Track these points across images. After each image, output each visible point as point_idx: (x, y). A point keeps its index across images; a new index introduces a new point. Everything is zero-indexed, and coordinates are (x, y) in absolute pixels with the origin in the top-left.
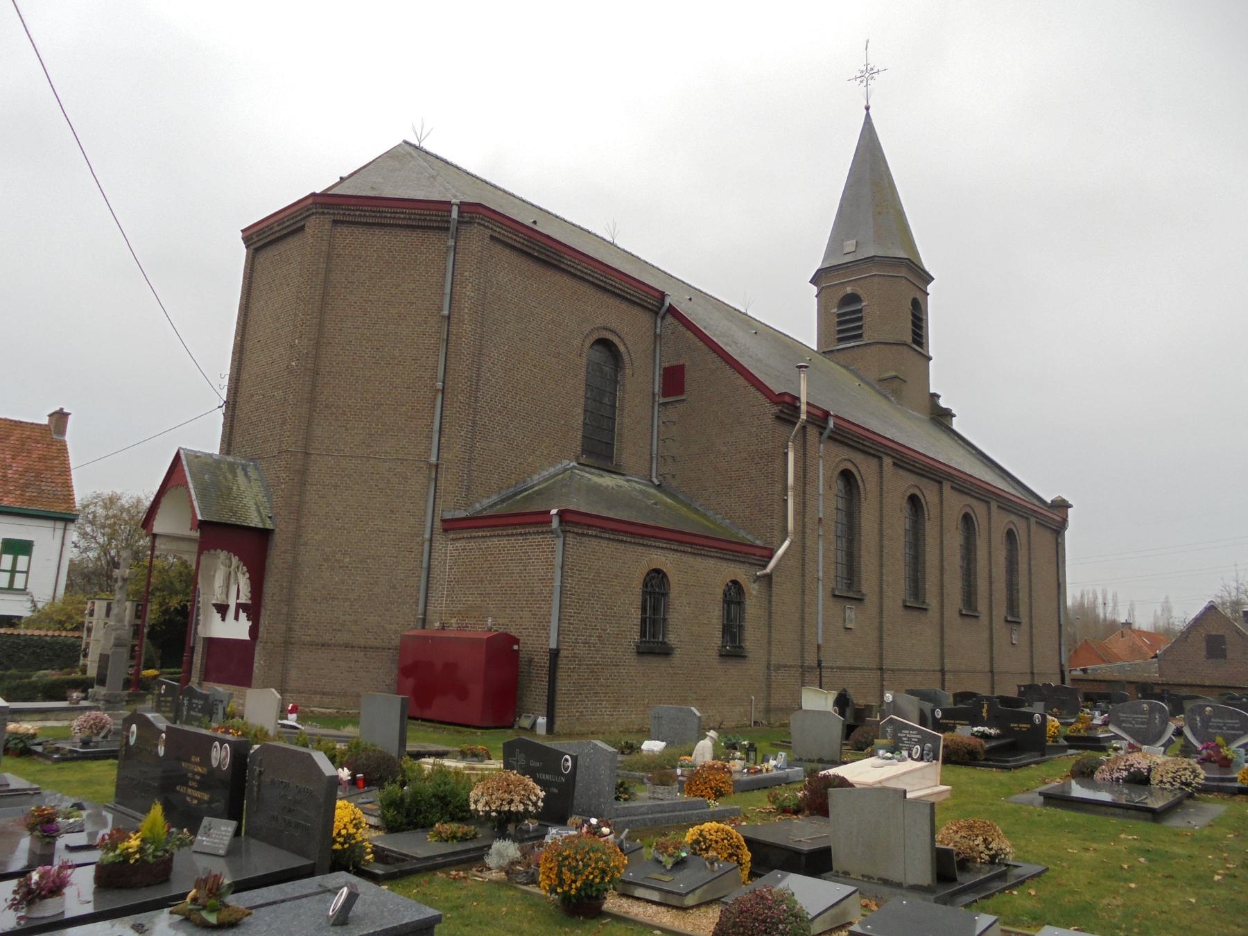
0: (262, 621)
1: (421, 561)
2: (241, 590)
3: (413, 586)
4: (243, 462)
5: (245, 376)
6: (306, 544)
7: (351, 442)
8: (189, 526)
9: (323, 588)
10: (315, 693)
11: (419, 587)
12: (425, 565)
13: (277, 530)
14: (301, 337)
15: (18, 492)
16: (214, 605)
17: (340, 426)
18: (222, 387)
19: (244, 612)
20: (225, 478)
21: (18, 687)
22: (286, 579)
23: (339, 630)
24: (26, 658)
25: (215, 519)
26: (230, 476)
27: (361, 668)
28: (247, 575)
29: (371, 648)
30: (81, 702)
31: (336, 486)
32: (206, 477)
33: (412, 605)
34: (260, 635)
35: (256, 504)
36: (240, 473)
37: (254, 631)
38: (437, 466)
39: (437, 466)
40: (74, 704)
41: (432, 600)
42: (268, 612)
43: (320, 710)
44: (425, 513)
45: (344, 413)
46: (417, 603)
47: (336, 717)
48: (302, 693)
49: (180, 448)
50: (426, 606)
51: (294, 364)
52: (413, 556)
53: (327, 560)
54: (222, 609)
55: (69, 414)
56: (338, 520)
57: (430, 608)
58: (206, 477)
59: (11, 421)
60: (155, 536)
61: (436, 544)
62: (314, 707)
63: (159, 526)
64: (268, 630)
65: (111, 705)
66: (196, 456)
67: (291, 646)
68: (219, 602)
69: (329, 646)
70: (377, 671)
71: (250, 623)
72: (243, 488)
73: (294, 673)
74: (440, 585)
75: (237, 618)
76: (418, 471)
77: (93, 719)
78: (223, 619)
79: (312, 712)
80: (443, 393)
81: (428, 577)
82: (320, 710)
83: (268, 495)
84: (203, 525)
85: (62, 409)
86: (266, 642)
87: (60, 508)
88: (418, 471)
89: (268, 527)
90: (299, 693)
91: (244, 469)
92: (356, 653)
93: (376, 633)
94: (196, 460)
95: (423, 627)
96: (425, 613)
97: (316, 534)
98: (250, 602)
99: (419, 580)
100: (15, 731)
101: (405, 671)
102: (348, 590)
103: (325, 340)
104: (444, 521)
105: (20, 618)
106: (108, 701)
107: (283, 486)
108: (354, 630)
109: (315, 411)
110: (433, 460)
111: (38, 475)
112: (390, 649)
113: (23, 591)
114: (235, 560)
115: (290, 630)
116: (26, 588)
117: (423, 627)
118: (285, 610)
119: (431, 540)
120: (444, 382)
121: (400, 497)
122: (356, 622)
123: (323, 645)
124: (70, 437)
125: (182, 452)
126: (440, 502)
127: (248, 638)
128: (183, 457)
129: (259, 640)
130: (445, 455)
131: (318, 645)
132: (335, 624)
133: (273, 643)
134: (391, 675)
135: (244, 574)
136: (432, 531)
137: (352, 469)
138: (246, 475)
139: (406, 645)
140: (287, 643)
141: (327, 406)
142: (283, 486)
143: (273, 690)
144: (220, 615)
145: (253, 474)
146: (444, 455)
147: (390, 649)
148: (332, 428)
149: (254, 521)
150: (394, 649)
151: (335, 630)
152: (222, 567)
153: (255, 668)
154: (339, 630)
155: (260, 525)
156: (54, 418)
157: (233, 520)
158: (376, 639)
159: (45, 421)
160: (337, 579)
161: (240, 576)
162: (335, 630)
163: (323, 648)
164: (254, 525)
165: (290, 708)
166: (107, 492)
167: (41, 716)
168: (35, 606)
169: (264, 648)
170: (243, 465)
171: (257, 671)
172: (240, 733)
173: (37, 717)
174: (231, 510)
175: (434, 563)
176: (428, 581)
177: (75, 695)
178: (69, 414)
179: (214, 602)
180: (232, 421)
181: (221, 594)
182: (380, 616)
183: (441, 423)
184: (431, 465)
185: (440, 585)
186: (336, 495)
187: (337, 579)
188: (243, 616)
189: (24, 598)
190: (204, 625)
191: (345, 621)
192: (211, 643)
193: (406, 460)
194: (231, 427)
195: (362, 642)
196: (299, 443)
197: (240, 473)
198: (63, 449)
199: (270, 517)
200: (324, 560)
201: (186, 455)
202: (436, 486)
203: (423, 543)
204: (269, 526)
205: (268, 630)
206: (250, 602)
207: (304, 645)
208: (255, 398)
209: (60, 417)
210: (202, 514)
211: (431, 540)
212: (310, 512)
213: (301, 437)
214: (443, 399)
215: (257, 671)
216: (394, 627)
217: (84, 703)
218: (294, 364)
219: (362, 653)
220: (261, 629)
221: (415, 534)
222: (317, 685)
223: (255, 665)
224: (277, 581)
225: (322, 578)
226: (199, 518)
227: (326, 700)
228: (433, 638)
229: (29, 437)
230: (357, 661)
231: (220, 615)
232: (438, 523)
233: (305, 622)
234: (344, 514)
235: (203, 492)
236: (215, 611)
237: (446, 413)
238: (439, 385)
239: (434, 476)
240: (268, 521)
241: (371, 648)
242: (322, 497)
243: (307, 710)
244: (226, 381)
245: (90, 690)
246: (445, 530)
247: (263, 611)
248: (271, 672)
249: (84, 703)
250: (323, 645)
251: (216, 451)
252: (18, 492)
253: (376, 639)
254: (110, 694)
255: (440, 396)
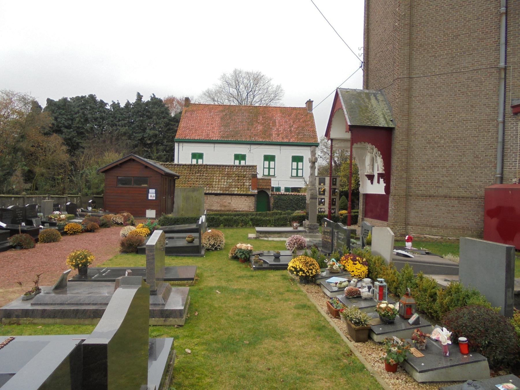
0: (392, 183)
1: (497, 138)
2: (379, 167)
3: (491, 156)
4: (374, 92)
5: (371, 45)
6: (415, 134)
7: (439, 65)
8: (345, 130)
9: (428, 160)
10: (427, 226)
11: (496, 155)
12: (500, 139)
13: (396, 127)
14: (399, 6)
15: (296, 136)
16: (367, 175)
17: (430, 56)
18: (360, 55)
19: (381, 178)
20: (364, 101)
21: (278, 219)
22: (404, 157)
23: (441, 187)
24: (302, 204)
25: (358, 124)
26: (367, 100)
27: (456, 211)
28: (381, 156)
29: (462, 198)
30: (298, 228)
31: (431, 95)
32: (353, 102)
33: (491, 169)
34: (391, 191)
35: (383, 114)
36: (372, 97)
37: (387, 189)
38: (505, 69)
39: (505, 69)
40: (295, 229)
41: (507, 164)
42: (395, 177)
43: (430, 236)
44: (498, 104)
45: (433, 47)
46: (495, 167)
47: (441, 242)
48: (418, 226)
49: (338, 88)
50: (502, 168)
51: (397, 24)
52: (490, 135)
53: (429, 143)
54: (371, 177)
55: (313, 101)
56: (435, 117)
57: (506, 170)
58: (353, 102)
59: (292, 108)
60: (332, 140)
61: (508, 125)
62: (426, 234)
63: (333, 135)
64: (395, 188)
65: (312, 230)
66: (347, 92)
67: (410, 197)
68: (368, 174)
69: (434, 197)
70: (468, 212)
71: (385, 185)
72: (374, 106)
73: (412, 214)
74: (514, 153)
75: (379, 182)
76: (490, 75)
77: (295, 239)
78: (372, 183)
79: (425, 237)
80: (506, 16)
81: (503, 148)
82: (430, 236)
83: (390, 108)
84: (352, 128)
85: (310, 100)
86: (395, 195)
87: (312, 141)
88: (490, 75)
89: (390, 126)
90: (417, 226)
91: (375, 95)
92: (452, 201)
93: (466, 187)
94: (347, 94)
95: (501, 182)
96: (502, 173)
97: (421, 127)
98: (384, 172)
99: (496, 151)
100: (240, 248)
101: (490, 213)
102: (445, 161)
103: (415, 4)
104: (513, 107)
105: (300, 188)
106: (310, 228)
107: (397, 100)
108: (451, 186)
109: (413, 50)
110: (502, 64)
111: (303, 129)
112: (477, 198)
113: (302, 177)
114: (375, 150)
115: (408, 187)
116: (303, 176)
117: (501, 182)
118: (405, 176)
119: (504, 122)
120: (507, 7)
121: (478, 95)
122: (451, 181)
123: (430, 196)
124: (314, 112)
125: (338, 90)
126: (509, 94)
127: (384, 193)
128: (339, 92)
129: (391, 194)
130: (512, 59)
131: (426, 196)
132: (437, 183)
133: (399, 196)
134: (478, 216)
135: (380, 156)
136: (504, 116)
137: (441, 83)
138: (376, 99)
139: (489, 194)
140: (408, 196)
141: (421, 46)
142: (397, 100)
143: (389, 228)
144: (370, 181)
145: (380, 98)
146: (511, 59)
147: (477, 198)
148: (426, 59)
149: (382, 123)
150: (480, 198)
151: (437, 187)
152: (369, 154)
153: (389, 210)
154: (441, 187)
155: (386, 126)
156: (307, 104)
157: (369, 124)
158: (466, 192)
159: (304, 106)
160: (436, 154)
161: (378, 157)
162: (437, 187)
163: (430, 198)
164: (382, 126)
165: (406, 238)
166: (229, 73)
167: (279, 235)
168: (306, 183)
169: (393, 199)
170: (374, 94)
171: (391, 212)
172: (364, 260)
173: (276, 235)
174: (368, 118)
175: (507, 138)
176: (503, 151)
177: (295, 224)
178: (313, 101)
179: (366, 174)
180: (367, 72)
181: (369, 169)
182: (468, 177)
183: (506, 38)
184: (500, 69)
185: (514, 153)
186: (432, 101)
187: (436, 154)
188: (381, 180)
189: (301, 180)
190: (363, 187)
191: (444, 181)
192: (366, 196)
193: (480, 69)
194: (367, 75)
195: (457, 195)
196: (405, 72)
197: (372, 97)
198: (312, 116)
199: (392, 121)
200: (428, 143)
201: (341, 92)
202: (505, 84)
203: (498, 125)
204: (391, 125)
205: (395, 188)
206: (384, 172)
207: (418, 196)
208: (378, 55)
209: (310, 103)
210: (350, 122)
211: (504, 122)
212: (416, 114)
213: (406, 68)
214: (506, 20)
215: (391, 212)
216: (478, 184)
217: (300, 229)
218: (397, 24)
219: (457, 201)
220: (392, 188)
221: (490, 119)
222: (427, 221)
223: (390, 209)
224: (399, 158)
225: (427, 154)
226: (349, 124)
227: (434, 230)
228: (512, 190)
229: (299, 113)
230: (454, 206)
231: (370, 181)
232: (509, 109)
233: (417, 182)
234: (438, 113)
235: (351, 111)
236: (367, 179)
237: (510, 29)
238: (503, 10)
239: (503, 76)
240: (391, 123)
241: (462, 198)
242: (423, 103)
243: (422, 236)
244: (362, 51)
245: (304, 222)
246: (516, 114)
247: (392, 176)
248: (398, 213)
249: (300, 229)
250: (430, 196)
251: (361, 88)
252: (296, 136)
253: (466, 192)
254: (311, 225)
255: (504, 18)
